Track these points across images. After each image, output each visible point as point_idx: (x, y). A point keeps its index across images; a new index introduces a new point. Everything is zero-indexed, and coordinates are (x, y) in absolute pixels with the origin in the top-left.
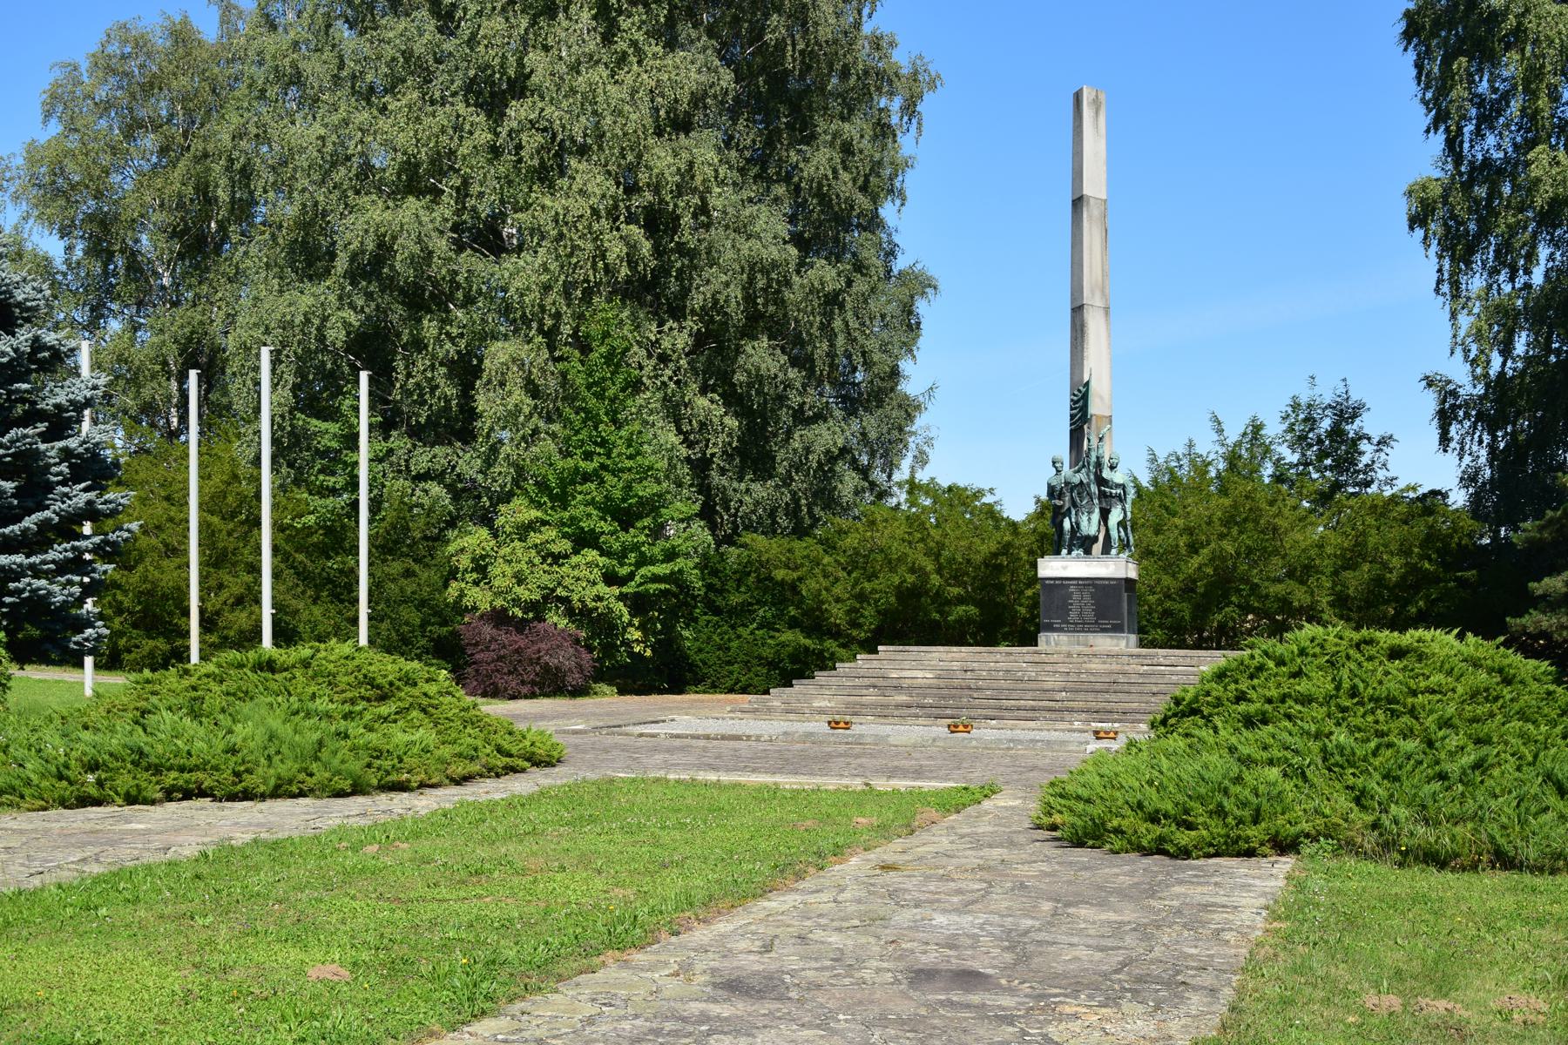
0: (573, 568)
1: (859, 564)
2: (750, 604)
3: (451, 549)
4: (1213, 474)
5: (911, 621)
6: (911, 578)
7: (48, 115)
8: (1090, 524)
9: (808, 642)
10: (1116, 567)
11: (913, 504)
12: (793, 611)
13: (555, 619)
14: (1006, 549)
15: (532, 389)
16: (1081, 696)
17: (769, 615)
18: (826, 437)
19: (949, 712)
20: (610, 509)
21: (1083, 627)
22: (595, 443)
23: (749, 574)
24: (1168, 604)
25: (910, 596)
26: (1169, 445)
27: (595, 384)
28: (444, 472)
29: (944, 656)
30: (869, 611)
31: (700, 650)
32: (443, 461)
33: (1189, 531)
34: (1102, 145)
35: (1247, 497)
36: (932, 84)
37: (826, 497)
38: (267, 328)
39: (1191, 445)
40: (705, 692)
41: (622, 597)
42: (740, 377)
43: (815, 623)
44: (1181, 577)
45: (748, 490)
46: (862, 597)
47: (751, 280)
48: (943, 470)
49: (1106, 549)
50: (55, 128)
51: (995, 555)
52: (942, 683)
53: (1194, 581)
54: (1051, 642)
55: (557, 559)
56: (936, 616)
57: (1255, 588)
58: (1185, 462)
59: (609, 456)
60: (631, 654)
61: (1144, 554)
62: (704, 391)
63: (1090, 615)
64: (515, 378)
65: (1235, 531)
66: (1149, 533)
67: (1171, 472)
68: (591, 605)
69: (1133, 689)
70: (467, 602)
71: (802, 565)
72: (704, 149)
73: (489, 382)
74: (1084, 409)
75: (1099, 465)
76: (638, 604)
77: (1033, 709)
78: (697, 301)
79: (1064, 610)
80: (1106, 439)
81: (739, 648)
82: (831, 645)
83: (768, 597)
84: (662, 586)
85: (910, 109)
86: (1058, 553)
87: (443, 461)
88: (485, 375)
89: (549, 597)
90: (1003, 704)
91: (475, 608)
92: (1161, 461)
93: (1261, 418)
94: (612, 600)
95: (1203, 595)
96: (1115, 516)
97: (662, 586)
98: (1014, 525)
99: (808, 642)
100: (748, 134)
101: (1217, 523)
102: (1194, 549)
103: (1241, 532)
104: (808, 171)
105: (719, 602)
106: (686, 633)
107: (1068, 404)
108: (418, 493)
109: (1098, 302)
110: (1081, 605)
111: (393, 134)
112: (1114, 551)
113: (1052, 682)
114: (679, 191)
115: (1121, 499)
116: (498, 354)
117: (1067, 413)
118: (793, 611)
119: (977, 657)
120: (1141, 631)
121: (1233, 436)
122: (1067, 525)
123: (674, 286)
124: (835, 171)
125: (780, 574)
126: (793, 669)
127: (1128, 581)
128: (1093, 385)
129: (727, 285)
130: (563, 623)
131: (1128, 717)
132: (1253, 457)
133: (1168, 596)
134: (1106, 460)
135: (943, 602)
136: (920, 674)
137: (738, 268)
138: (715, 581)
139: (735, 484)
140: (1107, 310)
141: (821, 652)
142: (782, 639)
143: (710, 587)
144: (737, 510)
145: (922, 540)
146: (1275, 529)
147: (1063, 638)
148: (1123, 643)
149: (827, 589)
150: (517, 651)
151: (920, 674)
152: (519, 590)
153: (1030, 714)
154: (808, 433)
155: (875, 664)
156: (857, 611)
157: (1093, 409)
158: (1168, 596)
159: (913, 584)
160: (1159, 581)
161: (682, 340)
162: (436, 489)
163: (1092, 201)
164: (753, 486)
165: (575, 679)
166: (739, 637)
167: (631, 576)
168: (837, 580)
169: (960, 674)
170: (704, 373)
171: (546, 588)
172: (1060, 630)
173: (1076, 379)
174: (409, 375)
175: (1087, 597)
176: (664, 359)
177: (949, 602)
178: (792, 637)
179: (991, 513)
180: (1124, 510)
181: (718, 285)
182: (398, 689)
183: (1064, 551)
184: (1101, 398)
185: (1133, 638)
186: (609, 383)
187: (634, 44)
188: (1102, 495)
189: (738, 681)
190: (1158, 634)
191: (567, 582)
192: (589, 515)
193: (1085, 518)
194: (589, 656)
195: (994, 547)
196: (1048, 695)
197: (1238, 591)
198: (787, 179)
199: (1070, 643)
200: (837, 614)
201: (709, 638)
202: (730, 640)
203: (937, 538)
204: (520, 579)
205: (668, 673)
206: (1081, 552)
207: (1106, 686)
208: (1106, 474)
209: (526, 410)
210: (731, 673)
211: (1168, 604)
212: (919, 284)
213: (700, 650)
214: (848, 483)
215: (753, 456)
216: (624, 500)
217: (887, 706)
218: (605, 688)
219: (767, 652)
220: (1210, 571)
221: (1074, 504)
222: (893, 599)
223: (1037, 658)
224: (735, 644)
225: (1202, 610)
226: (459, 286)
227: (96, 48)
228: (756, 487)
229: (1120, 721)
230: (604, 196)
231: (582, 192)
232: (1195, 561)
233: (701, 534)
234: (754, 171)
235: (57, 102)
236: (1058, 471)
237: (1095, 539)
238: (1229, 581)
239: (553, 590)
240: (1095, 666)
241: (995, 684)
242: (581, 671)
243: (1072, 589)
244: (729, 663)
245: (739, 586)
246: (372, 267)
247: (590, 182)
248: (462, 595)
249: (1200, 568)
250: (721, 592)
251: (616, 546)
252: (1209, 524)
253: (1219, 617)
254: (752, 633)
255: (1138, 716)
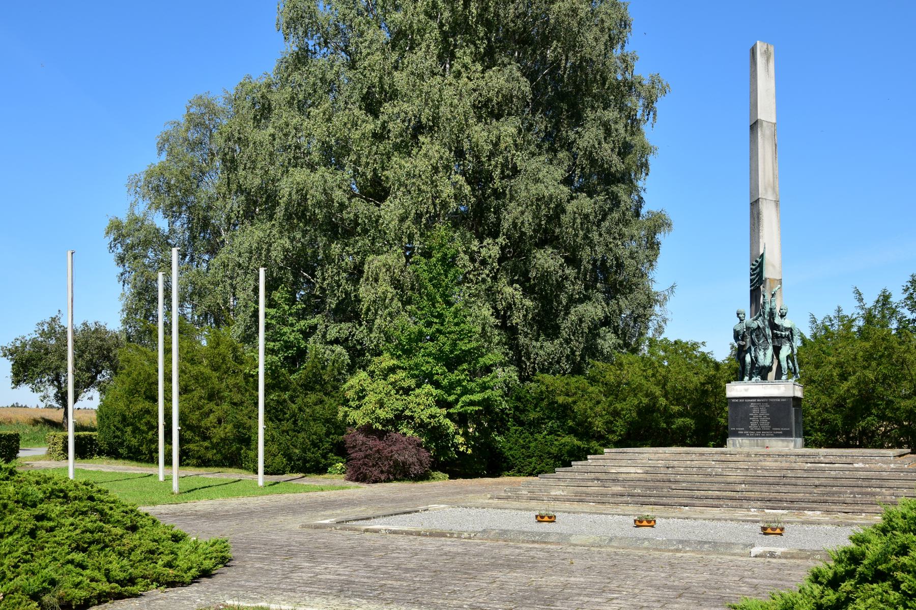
0: (416, 397)
1: (613, 391)
2: (543, 419)
3: (346, 386)
4: (855, 329)
5: (645, 430)
6: (645, 401)
7: (161, 150)
8: (765, 358)
9: (579, 443)
10: (785, 389)
11: (652, 354)
12: (570, 423)
13: (405, 430)
14: (711, 380)
15: (397, 284)
16: (757, 488)
17: (555, 426)
18: (593, 310)
19: (652, 500)
20: (441, 357)
21: (761, 433)
22: (433, 316)
23: (543, 400)
24: (826, 415)
25: (647, 411)
26: (824, 311)
27: (434, 278)
28: (347, 339)
29: (652, 456)
30: (620, 423)
31: (511, 449)
32: (346, 332)
33: (840, 365)
34: (773, 101)
35: (883, 339)
36: (664, 91)
37: (592, 350)
38: (240, 253)
39: (839, 311)
40: (513, 475)
41: (449, 416)
42: (533, 274)
43: (584, 431)
44: (835, 396)
45: (542, 347)
46: (616, 414)
47: (538, 207)
48: (671, 334)
49: (778, 376)
50: (164, 157)
51: (703, 384)
52: (648, 477)
53: (844, 399)
54: (737, 445)
55: (407, 391)
56: (665, 426)
57: (889, 403)
58: (835, 322)
59: (442, 325)
60: (458, 453)
61: (808, 382)
62: (511, 283)
63: (766, 424)
64: (383, 276)
65: (874, 364)
66: (811, 368)
67: (826, 329)
68: (427, 421)
69: (799, 482)
70: (350, 420)
71: (575, 393)
72: (508, 128)
73: (367, 279)
74: (760, 274)
75: (772, 314)
76: (461, 420)
77: (718, 498)
78: (506, 225)
79: (746, 421)
80: (778, 295)
81: (535, 447)
82: (594, 444)
83: (554, 415)
84: (477, 408)
85: (649, 106)
86: (742, 379)
87: (346, 332)
88: (365, 276)
89: (399, 417)
90: (692, 495)
91: (355, 423)
92: (819, 322)
93: (889, 290)
94: (441, 417)
95: (851, 409)
96: (785, 351)
97: (477, 408)
98: (717, 366)
99: (579, 443)
100: (541, 123)
101: (861, 359)
102: (844, 377)
103: (878, 365)
104: (582, 143)
105: (523, 417)
106: (498, 438)
107: (748, 272)
108: (328, 352)
109: (770, 196)
110: (759, 417)
111: (314, 130)
112: (784, 377)
113: (734, 476)
114: (492, 155)
115: (790, 339)
116: (374, 263)
117: (748, 278)
118: (570, 423)
119: (678, 457)
120: (806, 433)
121: (869, 302)
122: (748, 359)
123: (492, 217)
124: (599, 143)
125: (560, 399)
126: (565, 459)
127: (795, 399)
128: (766, 256)
129: (523, 213)
130: (410, 433)
131: (795, 505)
132: (884, 317)
133: (825, 410)
134: (777, 310)
135: (670, 417)
136: (632, 470)
137: (529, 203)
138: (519, 404)
139: (534, 343)
140: (777, 203)
141: (589, 449)
142: (563, 441)
143: (516, 408)
144: (535, 359)
145: (653, 375)
146: (904, 362)
147: (746, 441)
148: (792, 445)
149: (591, 409)
150: (378, 451)
151: (632, 470)
152: (378, 411)
153: (716, 502)
154: (581, 308)
155: (601, 462)
156: (611, 422)
157: (768, 273)
158: (825, 410)
159: (647, 405)
160: (818, 400)
161: (495, 251)
162: (339, 349)
163: (765, 124)
164: (545, 344)
165: (416, 469)
166: (536, 440)
167: (457, 401)
168: (598, 403)
169: (663, 470)
170: (511, 273)
171: (397, 410)
172: (744, 435)
173: (755, 253)
174: (324, 279)
175: (764, 411)
176: (484, 262)
177: (673, 416)
178: (571, 440)
179: (705, 358)
180: (792, 347)
181: (516, 214)
182: (12, 512)
183: (746, 378)
184: (773, 266)
185: (800, 441)
186: (443, 277)
187: (465, 66)
188: (775, 336)
189: (535, 468)
190: (819, 436)
191: (411, 406)
192: (428, 362)
193: (761, 353)
194: (427, 454)
195: (702, 379)
196: (731, 487)
197: (877, 405)
198: (569, 149)
199: (751, 446)
200: (599, 424)
201: (517, 441)
202: (530, 442)
203: (664, 373)
204: (381, 405)
205: (487, 462)
206: (759, 378)
207: (777, 480)
208: (778, 321)
209: (390, 296)
210: (531, 463)
211: (826, 415)
212: (659, 223)
213: (511, 449)
214: (608, 341)
215: (546, 324)
216: (452, 352)
217: (606, 495)
218: (440, 474)
219: (554, 450)
220: (855, 392)
221: (753, 343)
222: (634, 414)
223: (723, 458)
224: (533, 445)
225: (852, 417)
226: (358, 224)
227: (185, 113)
228: (547, 344)
229: (788, 508)
230: (441, 158)
231: (426, 155)
232: (845, 385)
233: (510, 374)
234: (546, 145)
235: (165, 143)
236: (741, 320)
237: (770, 369)
238: (869, 399)
239: (403, 411)
240: (769, 463)
241: (689, 478)
242: (421, 464)
243: (752, 405)
244: (529, 457)
245: (536, 407)
246: (299, 214)
247: (433, 149)
248: (346, 415)
249: (848, 390)
250: (523, 411)
251: (445, 382)
252: (855, 359)
253: (863, 424)
254: (544, 437)
255: (803, 505)
